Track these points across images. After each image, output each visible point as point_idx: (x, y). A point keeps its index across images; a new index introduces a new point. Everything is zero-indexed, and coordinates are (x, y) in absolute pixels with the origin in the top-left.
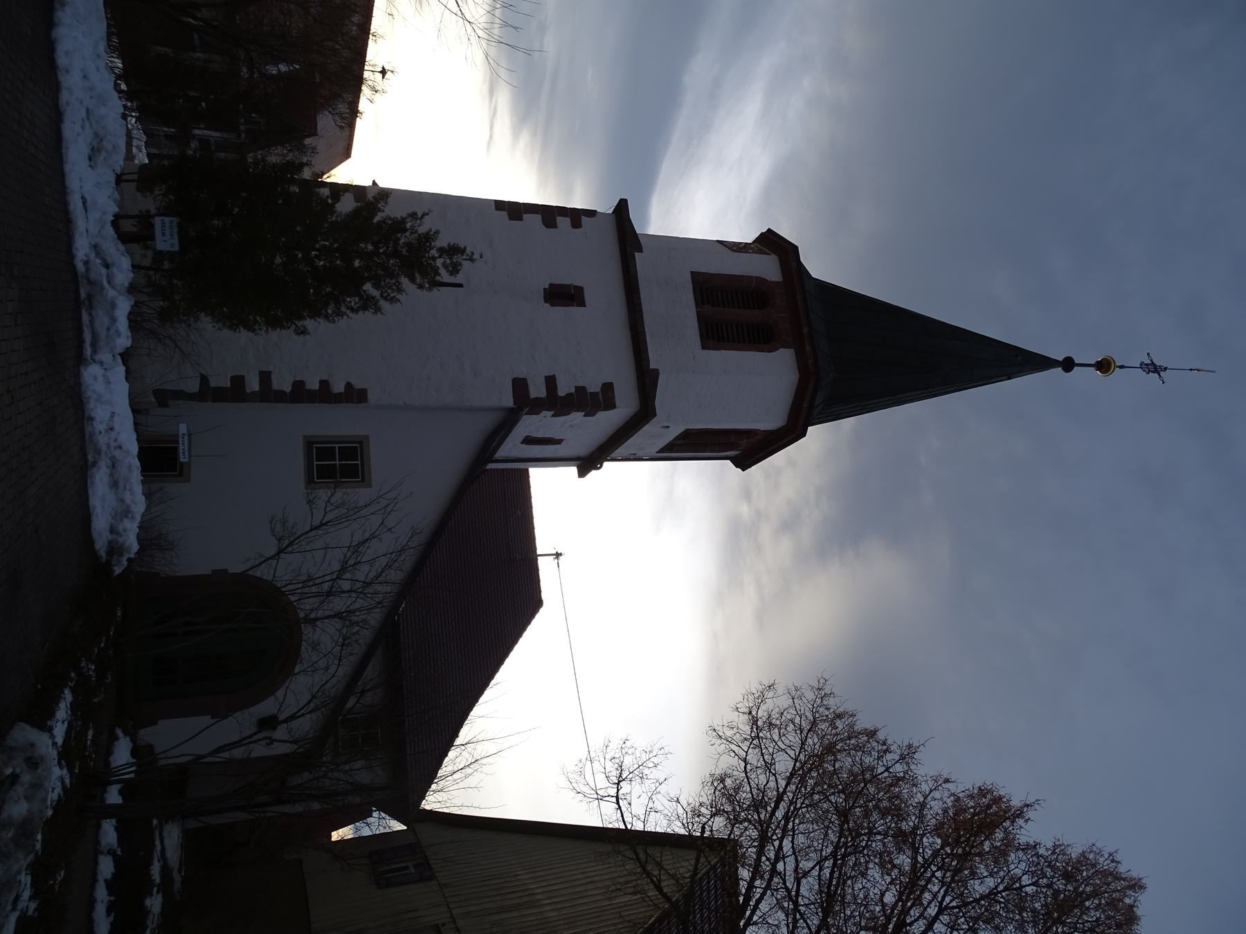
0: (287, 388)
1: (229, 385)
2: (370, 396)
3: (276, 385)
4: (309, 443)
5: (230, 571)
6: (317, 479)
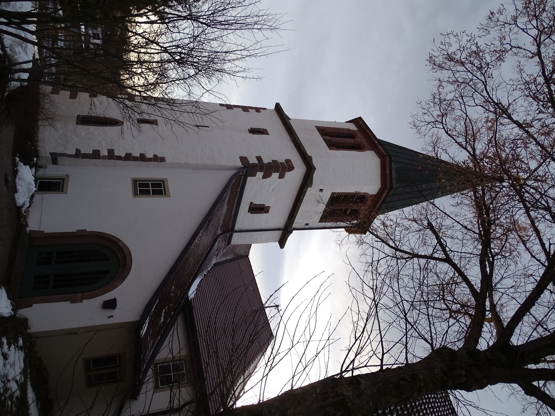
0: (123, 155)
1: (91, 152)
2: (166, 159)
3: (116, 153)
4: (135, 181)
5: (87, 231)
6: (159, 366)
